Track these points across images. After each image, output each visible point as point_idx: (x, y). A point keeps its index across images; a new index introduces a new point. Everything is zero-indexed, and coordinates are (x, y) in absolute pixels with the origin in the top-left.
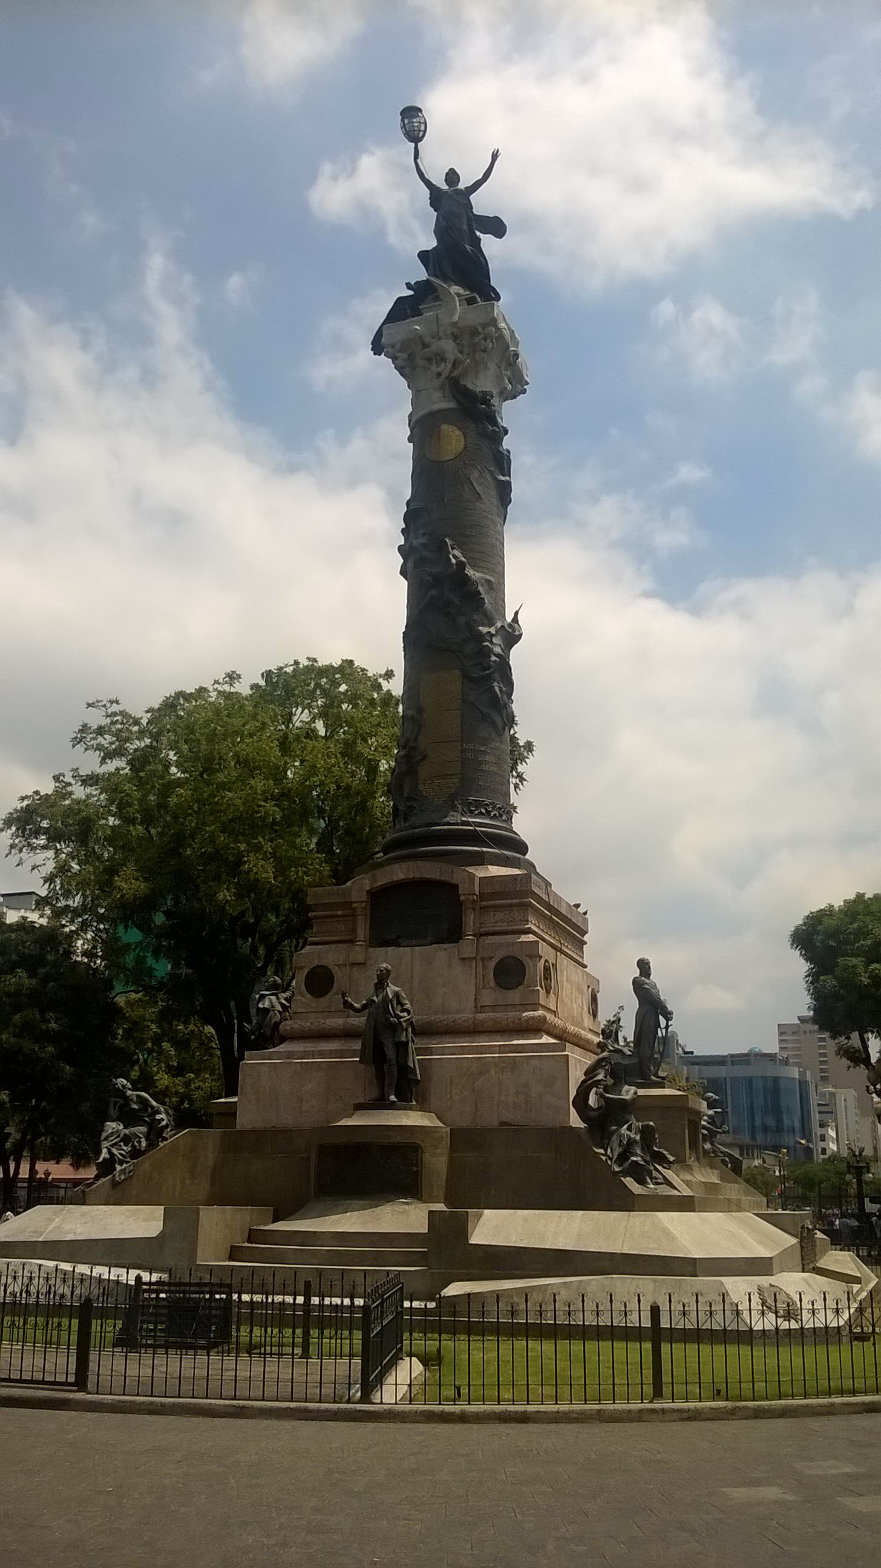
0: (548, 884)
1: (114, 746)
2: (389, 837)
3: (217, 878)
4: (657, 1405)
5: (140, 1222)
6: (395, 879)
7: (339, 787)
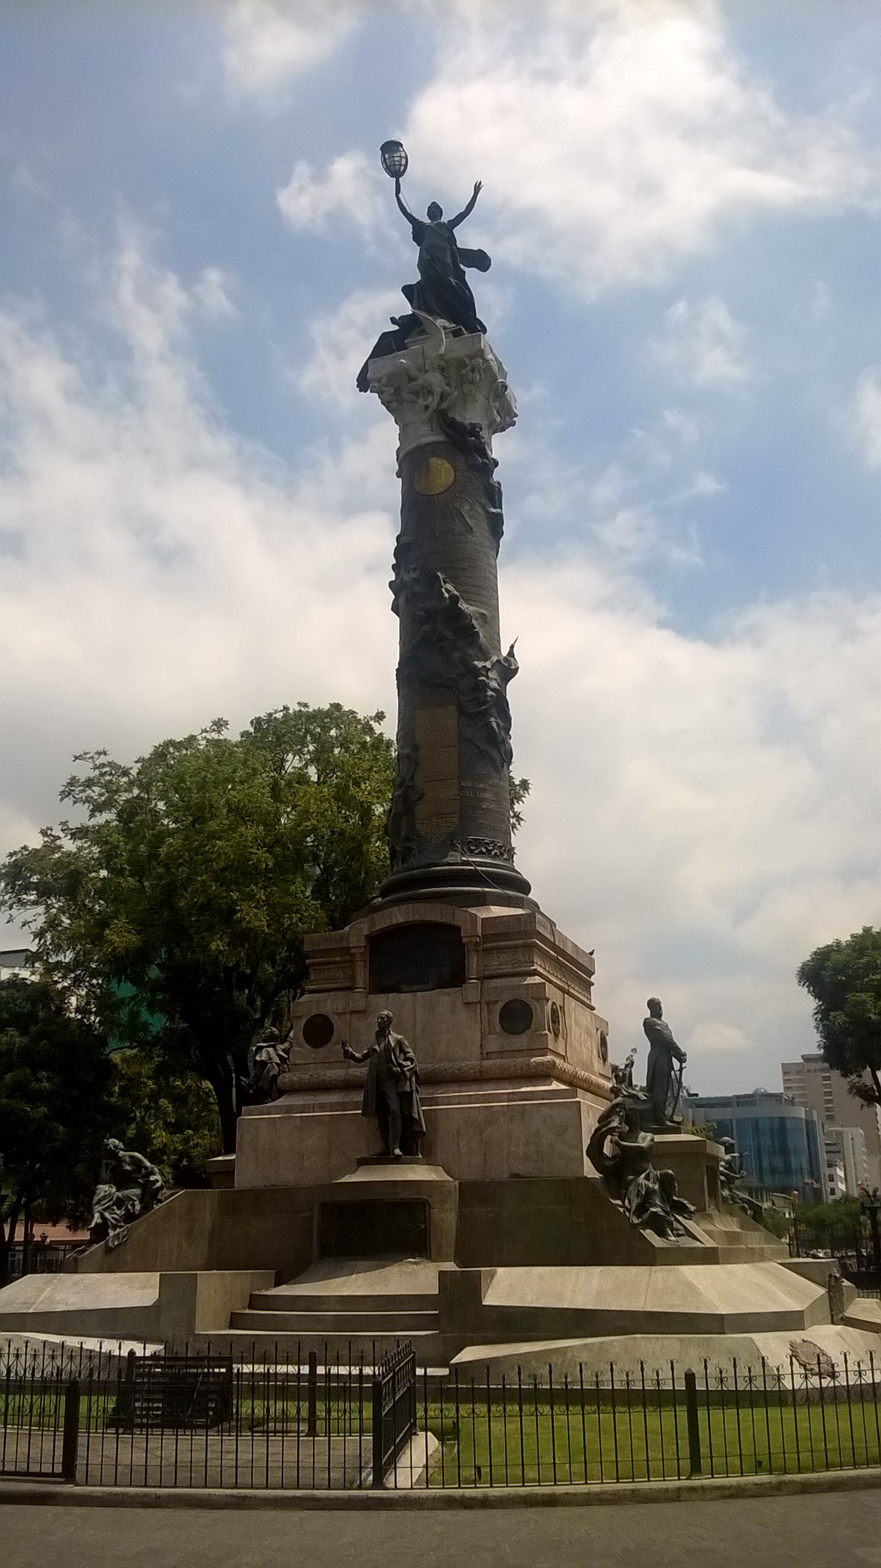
0: (552, 924)
1: (103, 798)
2: (385, 881)
3: (211, 928)
4: (696, 1482)
5: (134, 1290)
6: (395, 922)
7: (333, 832)
